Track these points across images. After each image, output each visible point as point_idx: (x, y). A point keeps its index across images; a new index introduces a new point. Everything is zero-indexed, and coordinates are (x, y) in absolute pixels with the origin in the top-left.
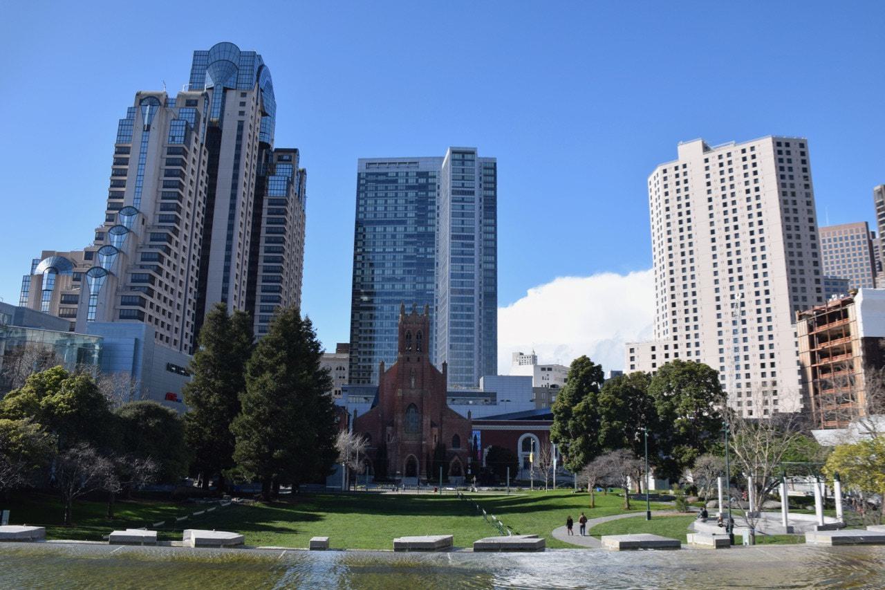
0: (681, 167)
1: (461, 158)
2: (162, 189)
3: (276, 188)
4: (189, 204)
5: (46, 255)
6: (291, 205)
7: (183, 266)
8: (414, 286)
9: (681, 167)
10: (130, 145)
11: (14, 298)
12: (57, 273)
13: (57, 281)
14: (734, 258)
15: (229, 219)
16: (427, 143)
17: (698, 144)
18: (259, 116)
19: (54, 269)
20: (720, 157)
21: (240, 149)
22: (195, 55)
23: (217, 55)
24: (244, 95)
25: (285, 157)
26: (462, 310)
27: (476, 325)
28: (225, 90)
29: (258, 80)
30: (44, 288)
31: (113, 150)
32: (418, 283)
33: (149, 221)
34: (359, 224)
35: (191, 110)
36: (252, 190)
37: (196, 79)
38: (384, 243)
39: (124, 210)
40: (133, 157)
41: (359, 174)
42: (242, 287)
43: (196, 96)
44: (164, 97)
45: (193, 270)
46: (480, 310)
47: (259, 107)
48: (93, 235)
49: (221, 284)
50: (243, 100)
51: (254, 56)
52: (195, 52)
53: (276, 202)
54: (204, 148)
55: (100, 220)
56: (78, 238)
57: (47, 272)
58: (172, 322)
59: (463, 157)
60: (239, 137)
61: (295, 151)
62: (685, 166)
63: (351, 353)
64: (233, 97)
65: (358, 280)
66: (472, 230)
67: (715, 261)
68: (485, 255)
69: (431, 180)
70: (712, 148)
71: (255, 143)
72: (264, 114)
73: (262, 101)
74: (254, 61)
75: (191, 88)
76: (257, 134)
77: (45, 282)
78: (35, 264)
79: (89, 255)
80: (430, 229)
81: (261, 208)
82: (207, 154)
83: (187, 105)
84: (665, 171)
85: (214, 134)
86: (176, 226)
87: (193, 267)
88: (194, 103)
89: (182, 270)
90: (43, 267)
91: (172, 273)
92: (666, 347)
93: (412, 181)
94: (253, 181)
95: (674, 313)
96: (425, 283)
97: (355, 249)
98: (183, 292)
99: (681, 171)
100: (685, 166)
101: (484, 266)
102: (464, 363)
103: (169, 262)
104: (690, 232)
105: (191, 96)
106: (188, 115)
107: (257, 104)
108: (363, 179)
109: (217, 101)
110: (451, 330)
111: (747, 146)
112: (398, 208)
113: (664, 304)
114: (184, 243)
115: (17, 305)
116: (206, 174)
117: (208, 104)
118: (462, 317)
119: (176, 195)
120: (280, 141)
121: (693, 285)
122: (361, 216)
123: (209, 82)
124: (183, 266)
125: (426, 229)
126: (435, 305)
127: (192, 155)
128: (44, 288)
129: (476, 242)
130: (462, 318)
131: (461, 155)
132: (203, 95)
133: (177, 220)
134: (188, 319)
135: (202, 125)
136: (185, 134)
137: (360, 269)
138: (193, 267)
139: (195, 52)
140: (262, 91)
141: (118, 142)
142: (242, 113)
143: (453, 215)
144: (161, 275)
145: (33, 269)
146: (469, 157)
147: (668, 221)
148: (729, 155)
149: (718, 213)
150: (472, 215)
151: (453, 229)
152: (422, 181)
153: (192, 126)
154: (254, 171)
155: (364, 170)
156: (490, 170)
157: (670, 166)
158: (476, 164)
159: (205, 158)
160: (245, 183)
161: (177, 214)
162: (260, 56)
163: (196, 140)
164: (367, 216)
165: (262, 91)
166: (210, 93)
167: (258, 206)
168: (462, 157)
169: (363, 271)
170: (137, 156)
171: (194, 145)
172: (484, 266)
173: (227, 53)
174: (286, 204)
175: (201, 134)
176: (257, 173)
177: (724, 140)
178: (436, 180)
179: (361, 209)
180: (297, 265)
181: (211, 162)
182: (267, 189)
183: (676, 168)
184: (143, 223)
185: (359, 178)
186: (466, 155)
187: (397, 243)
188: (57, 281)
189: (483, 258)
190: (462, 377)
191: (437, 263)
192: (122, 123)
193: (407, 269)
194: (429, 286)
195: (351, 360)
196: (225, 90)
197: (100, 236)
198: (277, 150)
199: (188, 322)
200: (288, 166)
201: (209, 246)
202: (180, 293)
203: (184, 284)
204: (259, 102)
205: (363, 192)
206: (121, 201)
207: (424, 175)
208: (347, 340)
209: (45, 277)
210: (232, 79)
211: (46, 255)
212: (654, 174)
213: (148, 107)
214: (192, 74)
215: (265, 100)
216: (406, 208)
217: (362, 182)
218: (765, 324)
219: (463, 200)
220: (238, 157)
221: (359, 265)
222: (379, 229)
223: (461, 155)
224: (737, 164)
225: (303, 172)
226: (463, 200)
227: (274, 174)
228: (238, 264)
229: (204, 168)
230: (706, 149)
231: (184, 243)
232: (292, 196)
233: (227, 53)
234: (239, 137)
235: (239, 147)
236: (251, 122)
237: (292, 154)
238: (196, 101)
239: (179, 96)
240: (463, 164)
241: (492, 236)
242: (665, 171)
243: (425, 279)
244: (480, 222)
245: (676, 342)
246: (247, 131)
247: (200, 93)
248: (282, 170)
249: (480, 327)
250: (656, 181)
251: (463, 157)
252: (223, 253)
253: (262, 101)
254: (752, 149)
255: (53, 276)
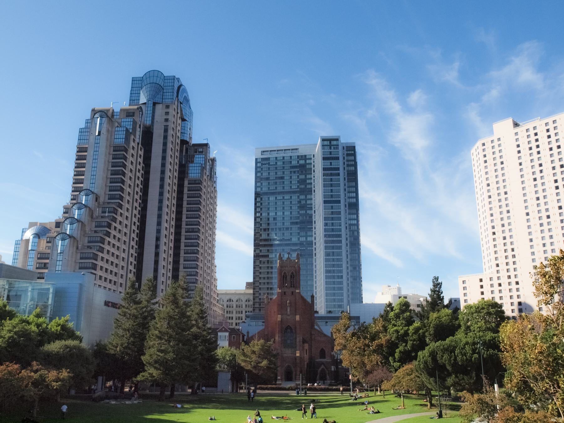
0: (496, 141)
1: (329, 144)
2: (108, 193)
3: (193, 172)
4: (130, 186)
5: (32, 225)
6: (205, 183)
7: (125, 255)
8: (299, 239)
9: (496, 141)
10: (87, 146)
11: (8, 261)
12: (39, 238)
13: (39, 243)
14: (541, 195)
15: (160, 188)
16: (306, 134)
17: (509, 122)
18: (179, 121)
19: (37, 235)
20: (527, 130)
21: (161, 218)
22: (133, 81)
23: (148, 79)
24: (168, 107)
25: (201, 150)
26: (333, 255)
27: (344, 266)
28: (155, 104)
29: (177, 96)
30: (30, 249)
31: (75, 150)
32: (301, 236)
33: (101, 200)
34: (257, 195)
35: (130, 119)
36: (176, 174)
37: (134, 99)
38: (276, 208)
39: (83, 192)
40: (89, 154)
41: (256, 159)
42: (172, 222)
43: (134, 109)
44: (111, 111)
45: (133, 240)
46: (347, 255)
47: (179, 115)
48: (62, 210)
49: (161, 161)
50: (167, 110)
51: (174, 79)
52: (133, 78)
53: (193, 182)
54: (140, 145)
55: (66, 200)
56: (51, 213)
57: (31, 237)
58: (118, 279)
59: (330, 143)
60: (165, 137)
61: (206, 145)
62: (499, 139)
63: (254, 289)
64: (160, 109)
65: (258, 220)
66: (339, 196)
67: (530, 230)
68: (349, 214)
69: (308, 161)
70: (520, 124)
71: (177, 140)
72: (183, 120)
73: (181, 111)
74: (174, 82)
75: (130, 105)
76: (179, 134)
77: (30, 244)
78: (23, 232)
79: (58, 224)
80: (308, 186)
81: (180, 242)
82: (143, 150)
83: (127, 116)
84: (484, 144)
85: (148, 134)
86: (120, 202)
87: (134, 230)
88: (132, 114)
89: (125, 233)
90: (29, 235)
91: (118, 235)
92: (491, 279)
93: (294, 163)
94: (177, 167)
95: (496, 252)
96: (306, 237)
97: (255, 214)
98: (127, 241)
99: (496, 143)
100: (499, 139)
101: (349, 222)
102: (336, 306)
103: (115, 228)
104: (507, 202)
105: (131, 109)
106: (128, 123)
107: (178, 113)
108: (259, 162)
109: (149, 112)
110: (325, 229)
111: (550, 120)
112: (285, 219)
113: (487, 240)
114: (126, 214)
115: (10, 264)
116: (142, 164)
117: (142, 114)
118: (333, 260)
119: (120, 180)
120: (196, 139)
121: (507, 205)
122: (259, 189)
123: (143, 99)
124: (125, 255)
125: (306, 186)
126: (314, 246)
127: (131, 151)
128: (30, 249)
129: (341, 171)
130: (334, 272)
131: (329, 142)
132: (138, 109)
133: (121, 198)
134: (131, 268)
135: (138, 129)
136: (126, 136)
137: (259, 207)
138: (134, 230)
139: (133, 78)
140: (181, 103)
141: (79, 144)
142: (167, 120)
143: (325, 186)
144: (109, 237)
145: (22, 235)
146: (334, 143)
147: (487, 176)
148: (535, 128)
149: (539, 252)
150: (339, 185)
151: (325, 196)
152: (302, 162)
153: (131, 131)
154: (177, 161)
155: (260, 156)
156: (351, 150)
157: (487, 140)
158: (340, 148)
159: (141, 153)
160: (171, 163)
161: (122, 185)
162: (178, 79)
163: (134, 140)
164: (263, 189)
165: (181, 103)
166: (143, 107)
167: (181, 186)
168: (330, 143)
169: (261, 214)
170: (92, 152)
171: (132, 144)
172: (349, 222)
173: (155, 78)
174: (200, 183)
175: (139, 133)
176: (179, 161)
177: (529, 117)
178: (312, 161)
179: (258, 215)
180: (210, 233)
181: (145, 166)
182: (188, 173)
183: (492, 141)
184: (96, 201)
185: (257, 162)
186: (332, 142)
187: (285, 208)
188: (39, 243)
189: (348, 217)
190: (335, 305)
191: (315, 222)
192: (81, 131)
193: (293, 170)
194: (309, 239)
195: (254, 294)
196: (155, 104)
197: (67, 210)
198: (195, 145)
199: (131, 270)
200: (202, 156)
201: (149, 171)
202: (124, 250)
203: (129, 227)
204: (179, 111)
205: (259, 172)
206: (82, 185)
207: (304, 157)
208: (251, 280)
209: (31, 241)
210: (159, 96)
211: (32, 225)
212: (475, 147)
213: (99, 119)
214: (131, 94)
215: (183, 110)
216: (291, 177)
217: (258, 170)
218: (511, 260)
219: (332, 196)
220: (164, 151)
221: (258, 210)
222: (272, 198)
223: (329, 142)
224: (542, 136)
225: (213, 160)
226: (331, 180)
227: (192, 162)
228: (166, 228)
229: (141, 160)
230: (516, 125)
231: (126, 214)
232: (205, 177)
233: (155, 78)
234: (165, 137)
235: (165, 144)
236: (172, 126)
237: (205, 147)
238: (134, 113)
239: (121, 110)
240: (330, 148)
241: (355, 222)
242: (484, 144)
243: (306, 196)
244: (345, 190)
245: (498, 275)
246: (170, 132)
247: (136, 107)
248: (199, 159)
249: (348, 268)
250: (477, 153)
251: (330, 143)
252: (156, 204)
253: (181, 111)
254: (554, 122)
255: (37, 240)
